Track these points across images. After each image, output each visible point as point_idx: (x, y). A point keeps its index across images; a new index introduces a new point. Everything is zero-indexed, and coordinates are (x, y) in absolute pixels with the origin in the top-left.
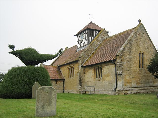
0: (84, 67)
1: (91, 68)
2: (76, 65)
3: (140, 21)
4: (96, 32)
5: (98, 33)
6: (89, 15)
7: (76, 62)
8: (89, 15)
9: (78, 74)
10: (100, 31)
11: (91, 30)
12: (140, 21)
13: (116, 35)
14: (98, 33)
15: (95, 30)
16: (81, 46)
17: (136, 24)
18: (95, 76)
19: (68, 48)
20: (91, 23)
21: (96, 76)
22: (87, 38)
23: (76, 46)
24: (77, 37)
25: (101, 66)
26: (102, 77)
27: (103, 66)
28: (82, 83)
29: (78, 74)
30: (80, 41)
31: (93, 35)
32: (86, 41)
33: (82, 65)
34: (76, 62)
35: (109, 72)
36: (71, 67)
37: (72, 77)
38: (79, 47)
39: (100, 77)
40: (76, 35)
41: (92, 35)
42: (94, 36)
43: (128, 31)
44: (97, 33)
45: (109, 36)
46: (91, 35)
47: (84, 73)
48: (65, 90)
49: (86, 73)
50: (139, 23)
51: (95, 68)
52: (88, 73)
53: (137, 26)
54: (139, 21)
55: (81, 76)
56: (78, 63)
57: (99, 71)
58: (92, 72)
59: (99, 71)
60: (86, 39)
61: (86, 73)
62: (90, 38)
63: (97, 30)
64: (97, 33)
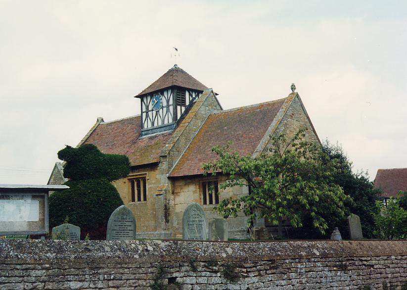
0: (173, 179)
1: (190, 181)
2: (153, 172)
3: (293, 87)
4: (191, 95)
5: (194, 96)
6: (177, 50)
7: (153, 166)
8: (177, 50)
9: (160, 195)
10: (199, 92)
11: (177, 88)
12: (293, 87)
13: (246, 108)
14: (194, 96)
15: (190, 90)
16: (163, 121)
17: (285, 93)
18: (200, 199)
19: (102, 120)
20: (175, 71)
21: (202, 200)
22: (171, 108)
23: (130, 121)
24: (142, 101)
25: (215, 180)
26: (145, 199)
27: (221, 180)
28: (169, 216)
29: (160, 195)
30: (150, 113)
31: (184, 101)
32: (161, 116)
33: (168, 175)
34: (153, 166)
35: (235, 193)
36: (136, 175)
37: (139, 200)
38: (160, 124)
39: (212, 203)
40: (141, 96)
41: (182, 102)
42: (187, 103)
43: (268, 104)
44: (192, 97)
45: (222, 109)
46: (180, 101)
47: (173, 193)
48: (138, 232)
49: (177, 193)
50: (291, 92)
51: (201, 184)
52: (182, 194)
53: (287, 96)
54: (292, 89)
55: (168, 198)
56: (159, 168)
57: (139, 186)
58: (195, 192)
59: (139, 186)
60: (168, 111)
61: (177, 193)
62: (179, 107)
63: (193, 90)
64: (192, 97)
